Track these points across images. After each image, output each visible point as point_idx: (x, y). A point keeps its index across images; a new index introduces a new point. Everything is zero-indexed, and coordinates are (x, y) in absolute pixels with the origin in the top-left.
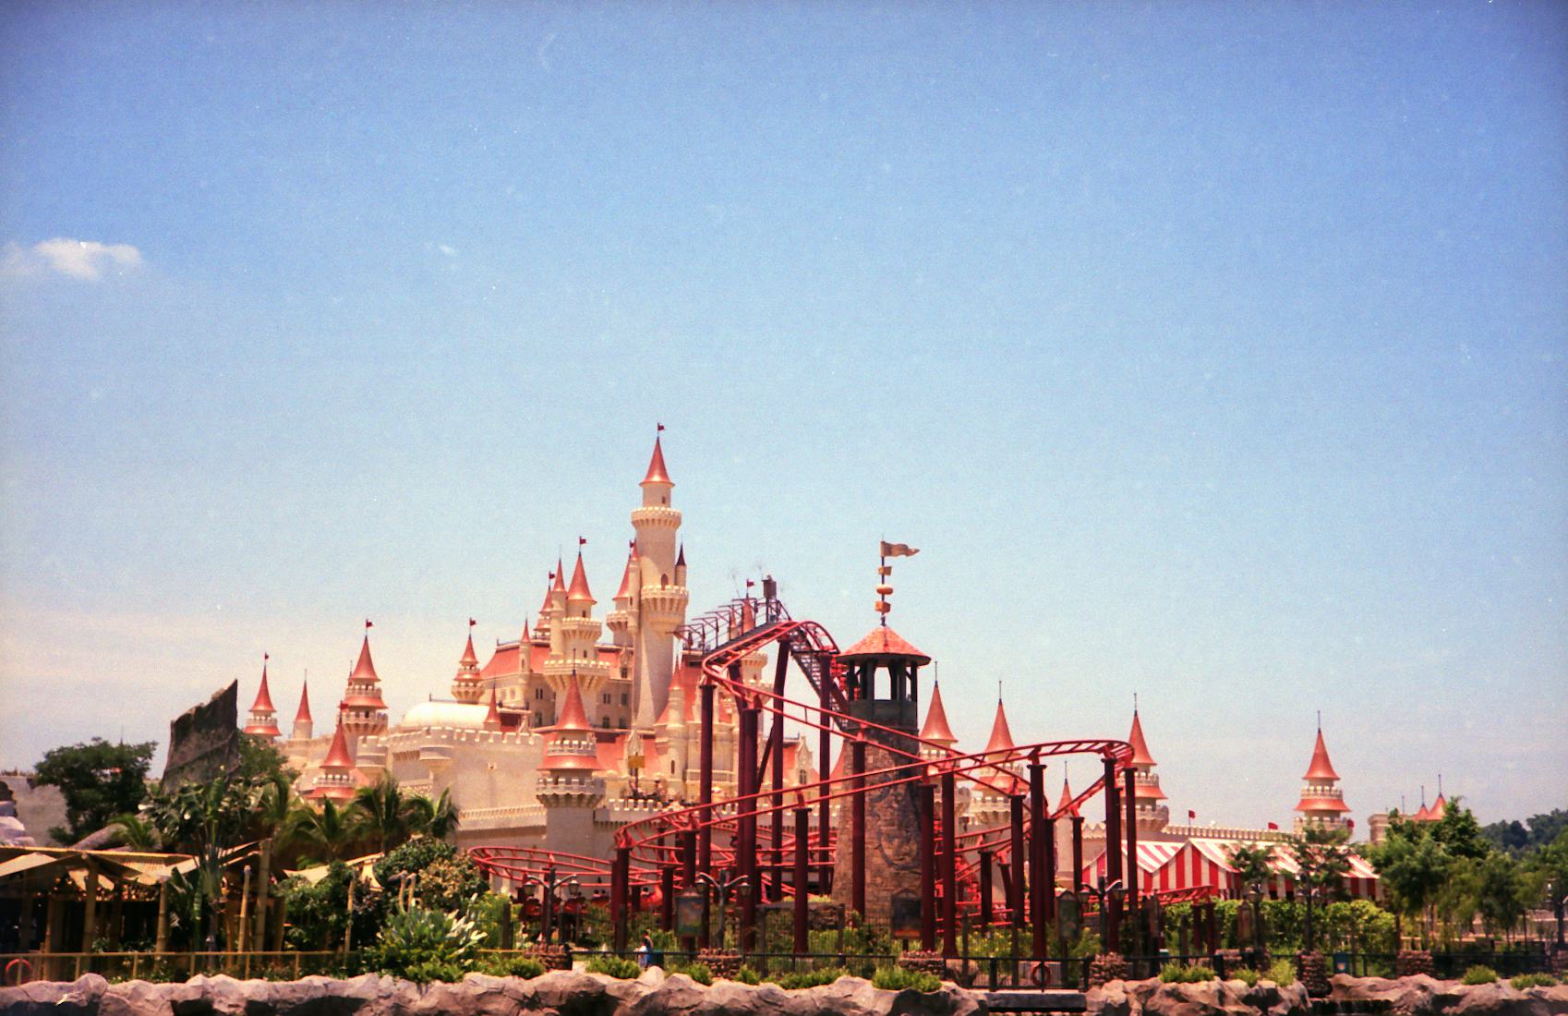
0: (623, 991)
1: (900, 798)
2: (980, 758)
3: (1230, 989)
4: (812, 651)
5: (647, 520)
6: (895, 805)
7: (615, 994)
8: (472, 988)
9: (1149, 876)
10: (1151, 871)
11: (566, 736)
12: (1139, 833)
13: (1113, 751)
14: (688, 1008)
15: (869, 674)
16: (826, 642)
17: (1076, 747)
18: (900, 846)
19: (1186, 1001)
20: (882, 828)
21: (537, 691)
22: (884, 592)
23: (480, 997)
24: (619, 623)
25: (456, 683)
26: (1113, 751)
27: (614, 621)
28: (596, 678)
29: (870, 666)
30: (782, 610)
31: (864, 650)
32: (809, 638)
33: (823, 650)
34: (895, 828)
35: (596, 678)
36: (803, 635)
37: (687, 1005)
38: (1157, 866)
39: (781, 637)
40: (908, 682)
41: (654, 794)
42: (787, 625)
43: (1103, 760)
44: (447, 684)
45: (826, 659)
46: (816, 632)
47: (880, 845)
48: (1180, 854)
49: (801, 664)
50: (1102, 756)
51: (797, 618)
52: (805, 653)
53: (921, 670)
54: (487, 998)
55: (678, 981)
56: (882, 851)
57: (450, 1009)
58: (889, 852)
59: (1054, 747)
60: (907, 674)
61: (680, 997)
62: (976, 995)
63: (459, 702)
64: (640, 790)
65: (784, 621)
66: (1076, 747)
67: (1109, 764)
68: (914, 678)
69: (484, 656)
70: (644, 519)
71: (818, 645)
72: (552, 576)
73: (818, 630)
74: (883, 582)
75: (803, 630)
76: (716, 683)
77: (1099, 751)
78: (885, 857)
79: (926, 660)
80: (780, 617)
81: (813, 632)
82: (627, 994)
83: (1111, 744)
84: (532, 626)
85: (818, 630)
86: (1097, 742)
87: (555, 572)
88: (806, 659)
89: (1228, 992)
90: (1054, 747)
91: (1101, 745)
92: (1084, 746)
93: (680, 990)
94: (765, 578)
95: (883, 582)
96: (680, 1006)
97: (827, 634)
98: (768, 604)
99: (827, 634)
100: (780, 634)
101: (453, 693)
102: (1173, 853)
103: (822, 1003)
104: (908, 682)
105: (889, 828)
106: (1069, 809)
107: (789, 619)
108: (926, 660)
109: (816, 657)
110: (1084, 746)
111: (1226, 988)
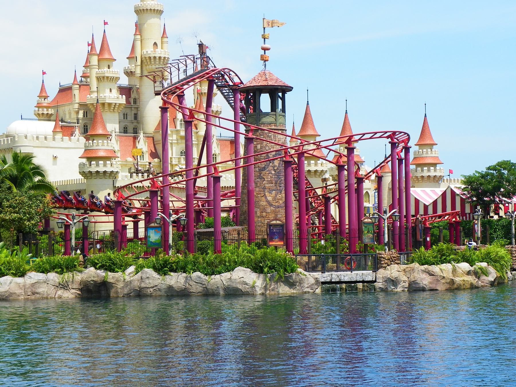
0: (115, 279)
1: (276, 168)
2: (318, 144)
3: (459, 267)
4: (229, 85)
5: (147, 9)
6: (273, 172)
7: (112, 281)
8: (29, 280)
9: (426, 207)
10: (427, 204)
11: (95, 138)
12: (411, 183)
13: (396, 137)
14: (153, 287)
15: (257, 97)
16: (236, 80)
17: (373, 135)
18: (276, 195)
19: (433, 275)
20: (266, 185)
21: (124, 114)
22: (265, 49)
23: (33, 285)
24: (131, 72)
25: (37, 109)
26: (396, 137)
27: (129, 71)
28: (118, 104)
29: (257, 94)
30: (210, 61)
31: (254, 84)
32: (226, 77)
33: (235, 84)
34: (273, 185)
35: (118, 104)
36: (223, 76)
37: (152, 286)
38: (431, 201)
39: (209, 77)
40: (280, 101)
41: (148, 170)
42: (213, 71)
43: (390, 142)
44: (31, 109)
45: (235, 89)
46: (230, 74)
47: (265, 195)
48: (444, 195)
49: (223, 93)
50: (390, 140)
51: (219, 67)
52: (226, 87)
53: (288, 95)
54: (37, 285)
55: (146, 273)
56: (266, 197)
57: (16, 292)
58: (270, 198)
59: (363, 138)
60: (279, 97)
61: (147, 281)
62: (314, 275)
63: (39, 120)
64: (140, 168)
65: (211, 69)
66: (373, 135)
67: (394, 145)
68: (283, 99)
69: (52, 92)
70: (149, 8)
71: (232, 82)
72: (89, 45)
73: (231, 73)
74: (264, 44)
75: (222, 74)
76: (169, 106)
77: (388, 137)
78: (268, 201)
79: (290, 89)
80: (209, 66)
81: (228, 74)
82: (118, 281)
83: (394, 133)
84: (79, 74)
85: (231, 73)
86: (386, 132)
87: (90, 42)
88: (226, 90)
89: (457, 269)
90: (363, 138)
91: (388, 134)
92: (378, 135)
93: (148, 278)
94: (199, 43)
95: (264, 44)
96: (147, 286)
97: (237, 75)
98: (202, 59)
99: (237, 75)
100: (208, 76)
101: (35, 114)
102: (440, 193)
103: (227, 282)
104: (280, 101)
105: (270, 185)
106: (375, 171)
107: (215, 67)
108: (290, 89)
109: (231, 89)
110: (378, 135)
111: (457, 267)
